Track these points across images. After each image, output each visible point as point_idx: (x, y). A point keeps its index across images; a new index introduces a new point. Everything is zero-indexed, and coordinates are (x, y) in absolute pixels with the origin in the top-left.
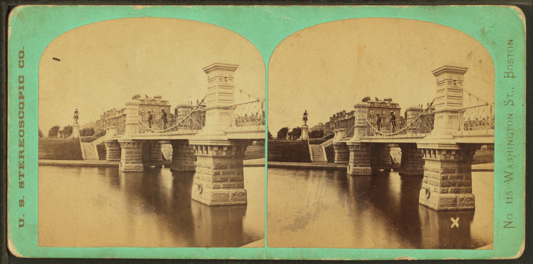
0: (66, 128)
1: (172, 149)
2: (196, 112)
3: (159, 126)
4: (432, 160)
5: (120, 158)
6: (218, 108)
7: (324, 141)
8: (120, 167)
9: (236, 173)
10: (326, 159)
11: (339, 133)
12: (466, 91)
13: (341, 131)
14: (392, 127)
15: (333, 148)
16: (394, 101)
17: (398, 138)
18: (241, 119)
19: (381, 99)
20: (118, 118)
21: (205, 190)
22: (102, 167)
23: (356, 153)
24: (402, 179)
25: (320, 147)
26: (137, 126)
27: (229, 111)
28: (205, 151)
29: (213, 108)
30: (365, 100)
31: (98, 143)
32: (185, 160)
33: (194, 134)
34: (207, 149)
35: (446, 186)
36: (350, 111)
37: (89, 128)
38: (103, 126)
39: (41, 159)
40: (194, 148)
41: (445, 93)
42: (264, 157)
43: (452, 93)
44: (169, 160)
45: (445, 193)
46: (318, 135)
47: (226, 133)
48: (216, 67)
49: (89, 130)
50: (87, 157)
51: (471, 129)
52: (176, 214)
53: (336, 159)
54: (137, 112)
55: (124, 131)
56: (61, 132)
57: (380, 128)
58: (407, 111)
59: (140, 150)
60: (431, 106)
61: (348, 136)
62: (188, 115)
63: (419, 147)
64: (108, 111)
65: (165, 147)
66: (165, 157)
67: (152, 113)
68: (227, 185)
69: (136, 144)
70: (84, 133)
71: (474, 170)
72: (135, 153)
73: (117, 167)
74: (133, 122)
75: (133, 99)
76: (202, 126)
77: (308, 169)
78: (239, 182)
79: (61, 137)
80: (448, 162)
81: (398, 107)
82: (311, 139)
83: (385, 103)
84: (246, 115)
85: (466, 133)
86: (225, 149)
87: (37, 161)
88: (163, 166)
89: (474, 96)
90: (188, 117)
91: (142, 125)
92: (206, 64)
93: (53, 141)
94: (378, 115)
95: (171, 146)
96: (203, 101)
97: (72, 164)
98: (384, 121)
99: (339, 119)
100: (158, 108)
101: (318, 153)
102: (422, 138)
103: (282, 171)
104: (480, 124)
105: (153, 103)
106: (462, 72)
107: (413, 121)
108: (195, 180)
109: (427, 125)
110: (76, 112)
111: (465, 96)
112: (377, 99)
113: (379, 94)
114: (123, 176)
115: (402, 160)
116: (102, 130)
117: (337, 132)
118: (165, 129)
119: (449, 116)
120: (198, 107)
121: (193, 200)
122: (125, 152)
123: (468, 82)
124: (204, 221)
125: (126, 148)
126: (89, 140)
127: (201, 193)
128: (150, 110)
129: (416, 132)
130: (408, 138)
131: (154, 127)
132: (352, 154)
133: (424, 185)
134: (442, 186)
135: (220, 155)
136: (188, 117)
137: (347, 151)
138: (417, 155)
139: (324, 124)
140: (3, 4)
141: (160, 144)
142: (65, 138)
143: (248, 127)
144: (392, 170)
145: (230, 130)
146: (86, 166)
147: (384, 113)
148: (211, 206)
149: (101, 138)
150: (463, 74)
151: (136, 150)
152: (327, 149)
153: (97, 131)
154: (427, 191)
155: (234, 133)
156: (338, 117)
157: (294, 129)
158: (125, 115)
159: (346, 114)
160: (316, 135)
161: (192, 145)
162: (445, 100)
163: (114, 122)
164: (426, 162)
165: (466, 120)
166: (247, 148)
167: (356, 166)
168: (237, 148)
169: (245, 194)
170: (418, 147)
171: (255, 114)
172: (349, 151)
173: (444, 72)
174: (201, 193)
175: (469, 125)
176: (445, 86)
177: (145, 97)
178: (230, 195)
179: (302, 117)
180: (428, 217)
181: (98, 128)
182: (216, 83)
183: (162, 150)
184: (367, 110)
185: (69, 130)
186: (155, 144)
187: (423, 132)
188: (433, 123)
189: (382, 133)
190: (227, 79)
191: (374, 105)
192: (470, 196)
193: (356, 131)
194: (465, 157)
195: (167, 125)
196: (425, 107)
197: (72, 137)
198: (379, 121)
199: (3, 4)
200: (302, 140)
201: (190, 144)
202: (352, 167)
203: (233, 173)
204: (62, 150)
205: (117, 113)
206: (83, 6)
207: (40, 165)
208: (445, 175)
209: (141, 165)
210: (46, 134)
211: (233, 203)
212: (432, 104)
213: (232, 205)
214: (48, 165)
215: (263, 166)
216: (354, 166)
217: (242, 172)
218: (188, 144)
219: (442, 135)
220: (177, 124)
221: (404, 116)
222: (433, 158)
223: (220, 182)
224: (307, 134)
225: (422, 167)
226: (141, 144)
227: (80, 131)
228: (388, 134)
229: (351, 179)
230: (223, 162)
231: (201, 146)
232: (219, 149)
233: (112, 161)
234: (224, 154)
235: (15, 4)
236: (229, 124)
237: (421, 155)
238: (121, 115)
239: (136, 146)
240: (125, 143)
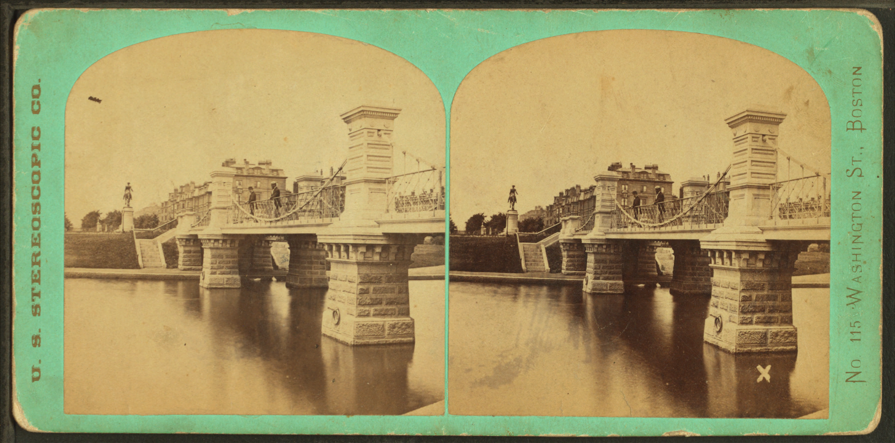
0: (111, 215)
1: (289, 251)
2: (329, 188)
3: (267, 212)
5: (202, 265)
6: (367, 181)
7: (545, 237)
8: (201, 280)
9: (397, 291)
11: (570, 222)
12: (783, 153)
13: (573, 219)
14: (659, 212)
15: (176, 244)
16: (661, 170)
17: (668, 232)
18: (404, 199)
19: (640, 166)
20: (198, 198)
21: (345, 318)
22: (171, 281)
23: (599, 257)
24: (675, 300)
25: (538, 247)
26: (231, 211)
27: (385, 186)
28: (343, 254)
29: (358, 182)
30: (614, 167)
31: (165, 241)
33: (327, 225)
34: (347, 251)
35: (749, 312)
36: (588, 187)
37: (150, 214)
38: (174, 212)
39: (69, 267)
40: (326, 248)
41: (747, 155)
43: (759, 155)
44: (285, 269)
45: (364, 316)
46: (533, 226)
47: (379, 224)
48: (363, 113)
49: (149, 218)
50: (147, 264)
51: (791, 217)
52: (295, 358)
53: (564, 267)
54: (230, 188)
55: (209, 219)
56: (102, 222)
57: (639, 215)
58: (684, 186)
59: (236, 252)
60: (723, 178)
61: (585, 229)
62: (315, 193)
63: (703, 246)
64: (182, 187)
65: (276, 246)
66: (278, 264)
67: (255, 190)
68: (382, 310)
69: (229, 242)
70: (140, 222)
71: (797, 286)
72: (227, 257)
73: (197, 280)
74: (223, 205)
75: (223, 165)
76: (339, 212)
77: (517, 284)
78: (402, 305)
79: (103, 230)
80: (753, 271)
81: (668, 180)
82: (522, 234)
84: (413, 193)
85: (782, 223)
86: (378, 250)
87: (62, 270)
88: (274, 279)
89: (795, 161)
92: (347, 107)
93: (89, 236)
94: (635, 193)
95: (287, 245)
96: (341, 169)
97: (122, 275)
98: (645, 203)
99: (570, 200)
100: (265, 181)
101: (534, 257)
102: (709, 231)
103: (473, 287)
104: (807, 209)
105: (257, 173)
106: (775, 120)
107: (694, 203)
108: (328, 303)
109: (718, 210)
110: (128, 188)
111: (782, 160)
112: (633, 167)
113: (636, 158)
114: (206, 296)
115: (675, 267)
116: (171, 219)
117: (565, 221)
118: (276, 216)
119: (754, 195)
120: (332, 180)
121: (324, 335)
122: (210, 256)
123: (787, 138)
124: (342, 370)
125: (211, 248)
126: (150, 234)
127: (338, 324)
128: (253, 185)
129: (698, 222)
130: (684, 231)
131: (258, 213)
132: (591, 258)
133: (712, 310)
134: (743, 312)
135: (370, 260)
138: (700, 260)
139: (544, 208)
140: (6, 6)
141: (268, 242)
142: (108, 231)
143: (417, 213)
144: (658, 285)
145: (387, 217)
146: (144, 278)
147: (646, 189)
148: (354, 346)
149: (170, 231)
150: (778, 123)
151: (229, 252)
152: (166, 246)
153: (163, 219)
154: (717, 321)
155: (393, 223)
156: (567, 197)
157: (494, 217)
158: (210, 193)
159: (581, 191)
160: (530, 226)
161: (323, 244)
163: (191, 204)
164: (715, 272)
165: (783, 201)
166: (415, 248)
167: (598, 278)
168: (398, 249)
169: (411, 326)
170: (702, 247)
171: (429, 192)
172: (586, 254)
173: (745, 122)
174: (338, 324)
175: (788, 211)
176: (748, 144)
177: (629, 166)
178: (387, 327)
179: (508, 196)
180: (718, 365)
181: (164, 214)
182: (364, 139)
183: (273, 251)
184: (616, 184)
185: (116, 219)
186: (260, 242)
187: (710, 222)
188: (727, 207)
189: (642, 224)
190: (381, 133)
192: (789, 328)
193: (598, 220)
194: (781, 264)
195: (280, 209)
196: (713, 180)
197: (120, 229)
198: (637, 203)
199: (6, 6)
200: (508, 235)
201: (319, 241)
202: (590, 281)
203: (392, 290)
204: (103, 252)
205: (197, 190)
206: (139, 10)
207: (67, 276)
208: (747, 294)
209: (237, 277)
210: (77, 224)
211: (391, 340)
212: (725, 174)
213: (390, 344)
214: (81, 277)
216: (595, 279)
217: (407, 289)
218: (316, 242)
219: (742, 226)
220: (297, 209)
221: (678, 195)
222: (727, 265)
223: (369, 305)
224: (516, 225)
225: (709, 280)
226: (237, 242)
227: (134, 220)
228: (651, 225)
229: (589, 300)
230: (375, 272)
232: (367, 250)
233: (188, 270)
234: (376, 258)
235: (25, 7)
236: (385, 208)
237: (707, 260)
238: (203, 192)
239: (228, 246)
240: (210, 240)
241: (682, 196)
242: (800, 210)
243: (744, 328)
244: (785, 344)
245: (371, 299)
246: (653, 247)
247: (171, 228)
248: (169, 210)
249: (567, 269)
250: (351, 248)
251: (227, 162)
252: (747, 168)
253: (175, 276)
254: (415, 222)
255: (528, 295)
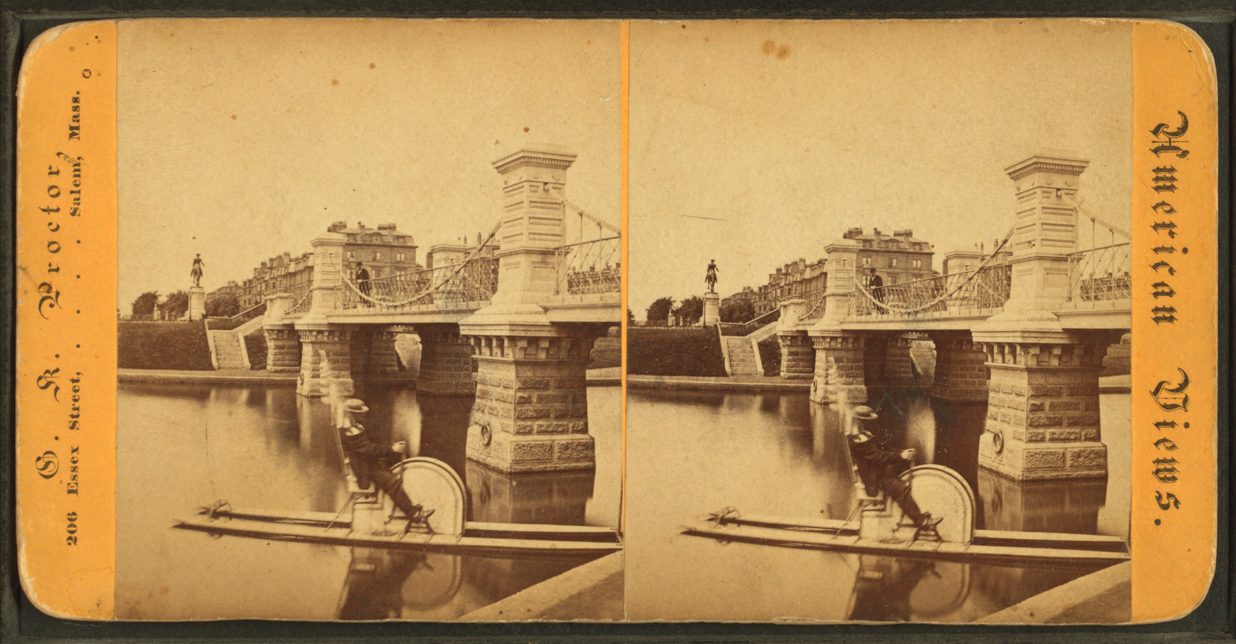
1: (420, 346)
2: (477, 261)
4: (1006, 369)
5: (300, 364)
6: (528, 252)
7: (243, 323)
8: (299, 386)
9: (1082, 407)
10: (760, 369)
11: (792, 308)
12: (1086, 213)
16: (401, 230)
21: (1010, 444)
25: (748, 342)
26: (340, 293)
27: (1067, 266)
28: (1009, 357)
32: (963, 376)
35: (1038, 426)
38: (260, 294)
40: (472, 342)
42: (619, 365)
43: (1053, 217)
45: (1037, 441)
48: (526, 160)
49: (226, 303)
50: (740, 370)
51: (1096, 298)
53: (784, 363)
54: (340, 260)
55: (310, 303)
56: (161, 307)
59: (347, 349)
60: (1001, 247)
63: (976, 338)
64: (272, 260)
65: (919, 346)
69: (337, 334)
71: (1108, 391)
75: (845, 237)
80: (536, 364)
81: (409, 244)
83: (897, 241)
84: (592, 269)
85: (1089, 306)
86: (1057, 352)
87: (113, 372)
89: (1101, 222)
90: (458, 272)
91: (351, 289)
92: (500, 153)
95: (418, 338)
96: (492, 235)
99: (791, 279)
104: (1118, 286)
105: (376, 241)
109: (996, 289)
110: (197, 261)
111: (571, 217)
112: (878, 233)
116: (257, 303)
117: (785, 306)
119: (1046, 269)
121: (982, 467)
123: (577, 186)
127: (1000, 452)
133: (989, 423)
136: (458, 272)
137: (294, 343)
138: (972, 356)
141: (906, 340)
142: (684, 325)
145: (1068, 307)
148: (1023, 481)
150: (565, 168)
152: (762, 345)
155: (1078, 315)
156: (786, 274)
157: (172, 297)
158: (311, 268)
160: (737, 314)
161: (468, 337)
162: (1036, 234)
165: (1086, 277)
166: (1109, 349)
168: (573, 346)
171: (614, 267)
174: (1000, 452)
175: (576, 283)
176: (525, 195)
177: (356, 226)
178: (1068, 457)
179: (705, 274)
181: (247, 297)
182: (1037, 201)
184: (854, 256)
185: (180, 302)
187: (986, 306)
191: (871, 246)
193: (830, 304)
194: (1084, 363)
196: (990, 250)
197: (187, 317)
199: (8, 15)
200: (705, 327)
201: (462, 333)
203: (1076, 407)
204: (162, 349)
205: (808, 270)
208: (1038, 402)
209: (863, 387)
212: (1005, 241)
213: (561, 471)
215: (617, 383)
217: (585, 396)
219: (1031, 309)
223: (531, 418)
225: (470, 376)
228: (903, 311)
231: (1001, 346)
234: (1055, 363)
236: (1066, 294)
237: (980, 356)
238: (301, 266)
240: (824, 338)
241: (430, 264)
242: (1110, 289)
243: (520, 438)
244: (1090, 468)
245: (1048, 418)
246: (391, 334)
247: (770, 322)
248: (254, 292)
249: (788, 371)
250: (506, 343)
251: (334, 226)
252: (524, 227)
253: (775, 387)
254: (1107, 314)
255: (217, 398)
